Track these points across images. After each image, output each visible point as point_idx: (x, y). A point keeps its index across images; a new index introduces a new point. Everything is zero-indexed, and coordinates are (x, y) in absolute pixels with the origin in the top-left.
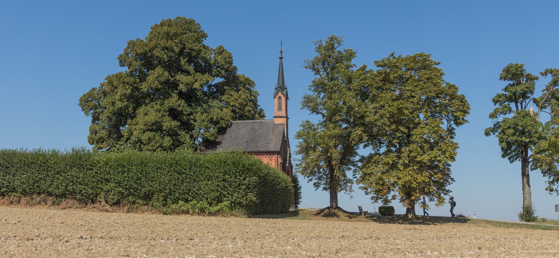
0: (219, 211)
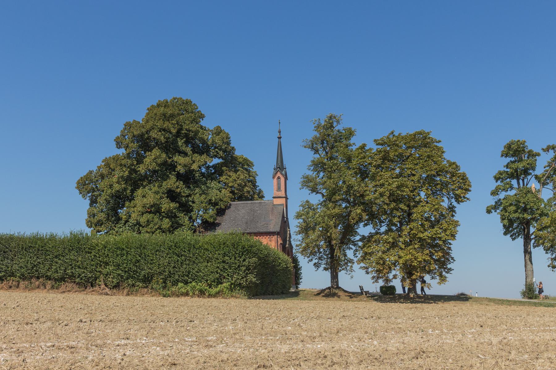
0: (219, 292)
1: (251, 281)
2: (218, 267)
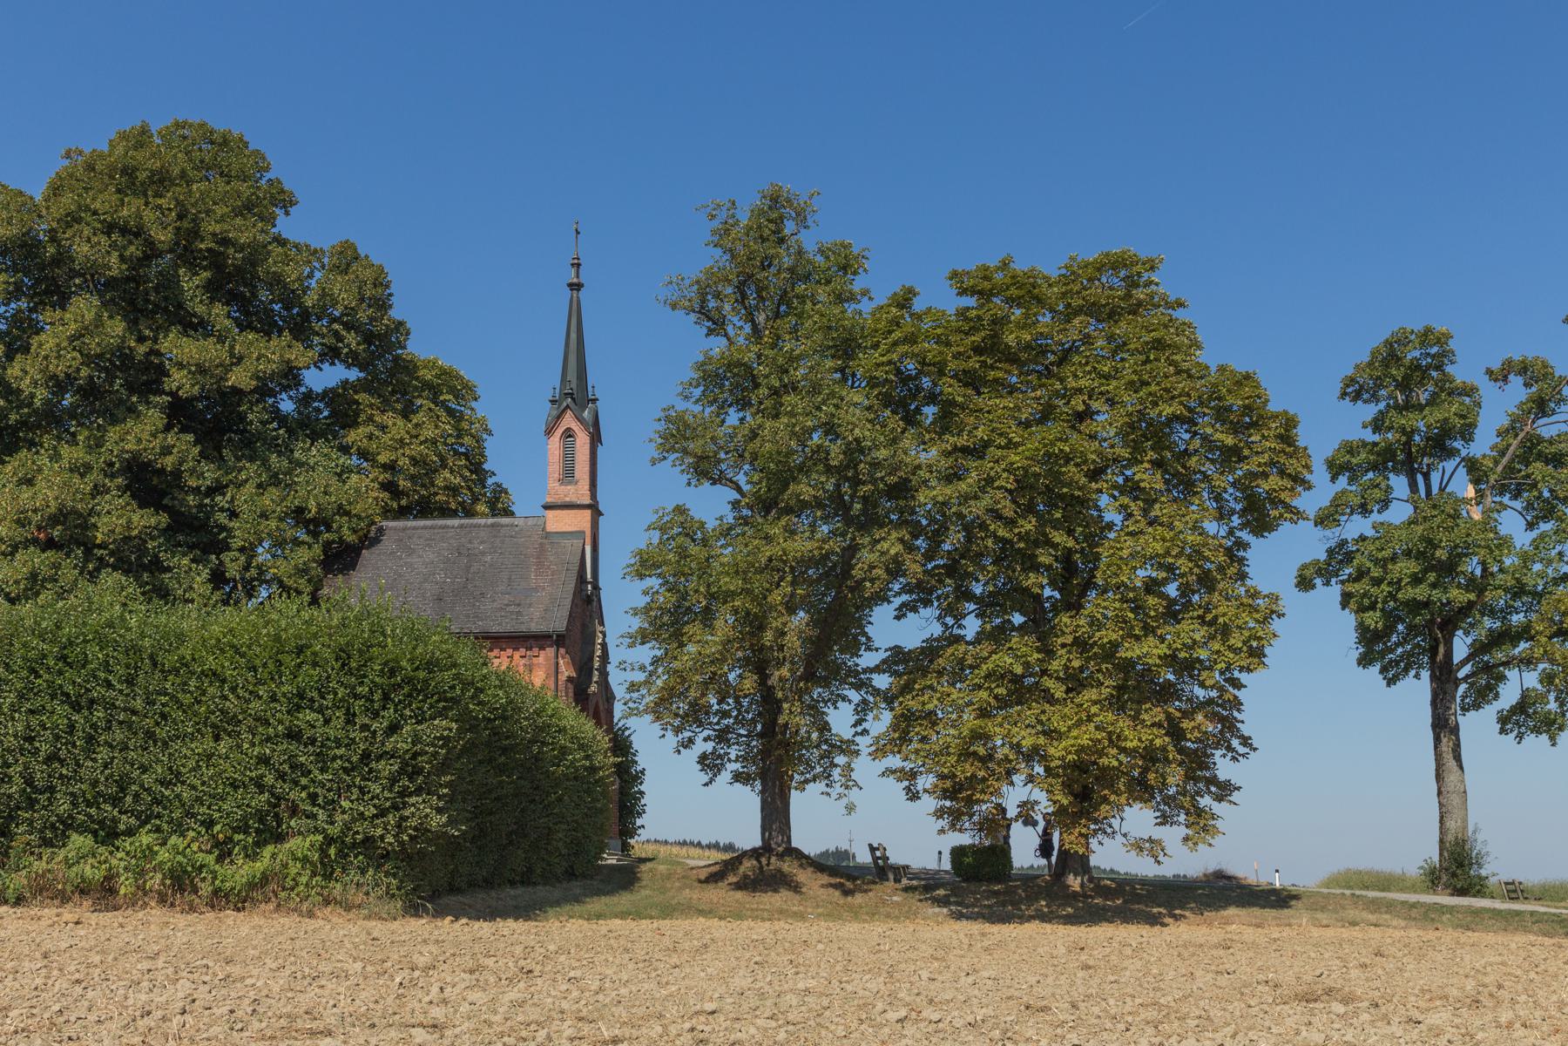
0: (265, 879)
1: (421, 830)
2: (264, 760)
